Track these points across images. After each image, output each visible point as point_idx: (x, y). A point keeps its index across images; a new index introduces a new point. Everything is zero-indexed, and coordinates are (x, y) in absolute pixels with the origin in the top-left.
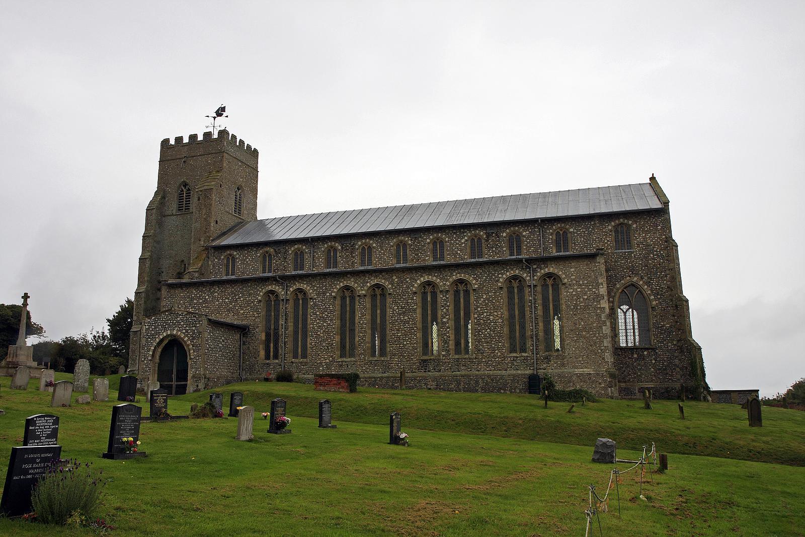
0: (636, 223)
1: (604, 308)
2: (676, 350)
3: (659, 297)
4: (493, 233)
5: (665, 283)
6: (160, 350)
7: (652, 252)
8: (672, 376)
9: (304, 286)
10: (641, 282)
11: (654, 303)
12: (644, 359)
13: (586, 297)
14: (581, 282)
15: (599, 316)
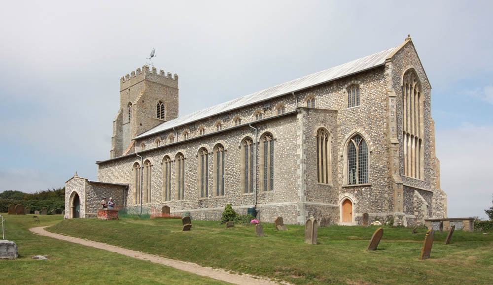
1: (299, 155)
2: (386, 186)
3: (376, 142)
4: (268, 108)
8: (381, 207)
10: (364, 132)
12: (362, 194)
13: (288, 148)
14: (286, 137)
15: (295, 162)
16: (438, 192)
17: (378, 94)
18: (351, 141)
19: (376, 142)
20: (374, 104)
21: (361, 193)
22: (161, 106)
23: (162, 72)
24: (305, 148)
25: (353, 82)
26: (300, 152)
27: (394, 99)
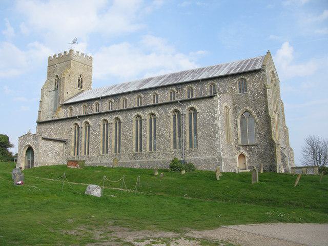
0: (249, 77)
5: (263, 109)
6: (25, 152)
7: (256, 92)
9: (88, 120)
11: (257, 120)
20: (256, 92)
21: (251, 150)
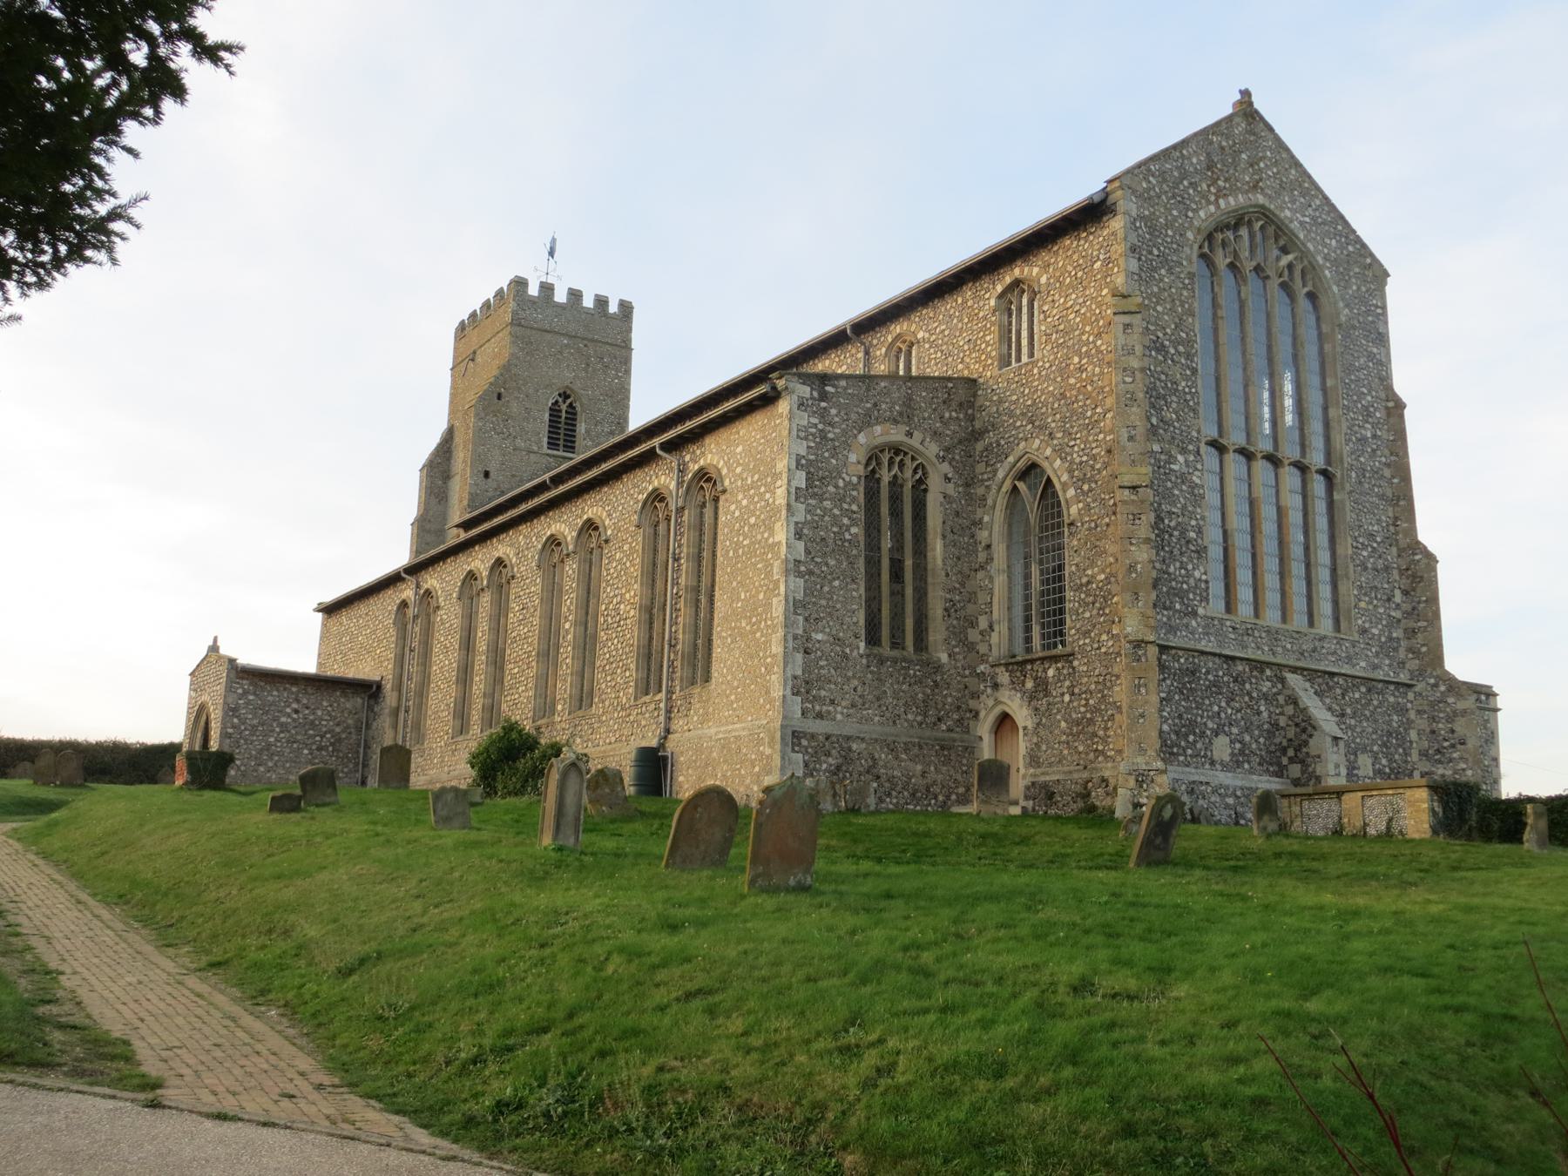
10: (1048, 452)
16: (1436, 685)
17: (1090, 309)
18: (1015, 488)
19: (1086, 487)
22: (564, 407)
23: (575, 295)
24: (800, 516)
25: (1017, 272)
26: (781, 534)
27: (1136, 320)
